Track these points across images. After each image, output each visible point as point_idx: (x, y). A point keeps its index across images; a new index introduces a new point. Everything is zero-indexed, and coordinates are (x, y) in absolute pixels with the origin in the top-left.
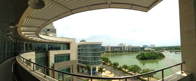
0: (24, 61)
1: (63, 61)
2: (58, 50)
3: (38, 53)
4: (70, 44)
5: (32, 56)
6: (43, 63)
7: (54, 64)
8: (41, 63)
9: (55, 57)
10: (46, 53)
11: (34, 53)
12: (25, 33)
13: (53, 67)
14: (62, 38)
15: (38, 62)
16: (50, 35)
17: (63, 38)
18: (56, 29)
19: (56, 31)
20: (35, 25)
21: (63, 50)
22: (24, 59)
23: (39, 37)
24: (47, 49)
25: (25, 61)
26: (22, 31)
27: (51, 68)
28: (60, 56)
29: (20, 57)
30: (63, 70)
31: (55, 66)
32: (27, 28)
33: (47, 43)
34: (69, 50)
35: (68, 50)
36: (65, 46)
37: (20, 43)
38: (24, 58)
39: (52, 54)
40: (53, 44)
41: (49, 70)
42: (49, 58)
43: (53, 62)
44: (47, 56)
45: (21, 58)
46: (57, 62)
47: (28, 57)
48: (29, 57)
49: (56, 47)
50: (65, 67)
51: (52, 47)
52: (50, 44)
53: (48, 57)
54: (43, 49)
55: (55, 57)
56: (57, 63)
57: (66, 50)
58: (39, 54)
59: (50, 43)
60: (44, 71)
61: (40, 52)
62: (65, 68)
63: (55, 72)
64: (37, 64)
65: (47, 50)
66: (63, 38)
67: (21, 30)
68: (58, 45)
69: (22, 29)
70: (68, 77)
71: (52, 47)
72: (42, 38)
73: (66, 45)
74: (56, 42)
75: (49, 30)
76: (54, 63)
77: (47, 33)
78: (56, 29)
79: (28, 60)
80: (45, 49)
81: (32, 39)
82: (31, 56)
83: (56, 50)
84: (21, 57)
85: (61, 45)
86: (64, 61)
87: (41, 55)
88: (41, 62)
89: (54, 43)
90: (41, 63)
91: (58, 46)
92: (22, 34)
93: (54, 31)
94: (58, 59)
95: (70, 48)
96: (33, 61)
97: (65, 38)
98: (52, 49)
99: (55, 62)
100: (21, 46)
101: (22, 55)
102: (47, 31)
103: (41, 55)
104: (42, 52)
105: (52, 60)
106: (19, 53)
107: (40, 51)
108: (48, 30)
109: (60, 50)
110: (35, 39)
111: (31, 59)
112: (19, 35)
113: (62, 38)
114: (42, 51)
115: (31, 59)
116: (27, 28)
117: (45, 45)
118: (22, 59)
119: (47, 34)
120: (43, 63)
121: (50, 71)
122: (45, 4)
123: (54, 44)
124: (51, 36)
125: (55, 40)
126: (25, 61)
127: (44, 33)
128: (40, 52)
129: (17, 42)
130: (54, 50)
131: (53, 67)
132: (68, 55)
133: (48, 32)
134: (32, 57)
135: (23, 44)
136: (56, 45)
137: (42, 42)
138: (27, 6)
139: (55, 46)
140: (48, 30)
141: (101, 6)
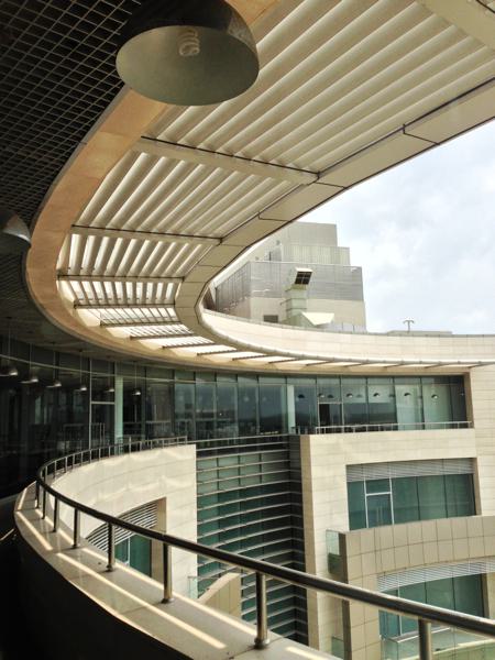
0: (84, 532)
1: (420, 519)
2: (372, 429)
3: (241, 450)
4: (469, 381)
5: (172, 477)
6: (263, 532)
7: (342, 537)
8: (243, 544)
9: (353, 488)
10: (287, 455)
11: (186, 454)
12: (96, 291)
13: (337, 564)
14: (400, 334)
15: (221, 537)
16: (315, 317)
17: (409, 333)
18: (359, 269)
19: (360, 286)
20: (172, 221)
21: (417, 428)
22: (83, 516)
23: (201, 329)
24: (292, 423)
25: (89, 525)
26: (63, 275)
27: (320, 571)
28: (391, 474)
29: (52, 499)
30: (426, 590)
31: (349, 553)
32: (91, 239)
33: (286, 376)
34: (465, 426)
35: (453, 426)
36: (427, 395)
37: (46, 380)
38: (79, 508)
39: (329, 462)
40: (336, 381)
41: (310, 590)
42: (305, 494)
43: (343, 524)
44: (289, 475)
45: (61, 504)
46: (374, 524)
47: (140, 489)
48: (151, 487)
49: (358, 405)
50: (440, 564)
51: (324, 409)
52: (312, 381)
53: (298, 487)
54: (257, 428)
55: (349, 484)
56: (367, 534)
57: (441, 427)
58: (228, 462)
59: (315, 377)
60: (254, 608)
61: (212, 444)
62: (445, 574)
63: (356, 607)
64: (214, 547)
65: (292, 432)
66: (409, 333)
67: (59, 266)
68: (379, 395)
69: (73, 250)
70: (462, 645)
71: (324, 409)
72: (218, 339)
73: (442, 389)
74: (354, 370)
75: (306, 282)
76: (344, 527)
77: (295, 303)
78: (359, 269)
79: (115, 514)
80: (277, 423)
81: (166, 354)
82: (164, 479)
83: (363, 430)
84: (58, 497)
85: (401, 389)
86: (427, 518)
87: (247, 469)
88: (243, 518)
89: (339, 377)
90: (243, 544)
91: (373, 400)
92: (56, 295)
93: (349, 286)
94: (377, 498)
95: (475, 417)
96: (182, 521)
97: (427, 335)
98: (329, 419)
99: (356, 520)
100: (85, 404)
101: (63, 483)
102: (139, 141)
103: (247, 469)
104: (254, 449)
105: (327, 513)
106: (41, 463)
107: (219, 443)
108: (303, 279)
109: (396, 429)
110: (189, 349)
111: (164, 500)
112: (38, 315)
113: (400, 334)
114: (254, 441)
115: (164, 500)
116: (91, 239)
117: (276, 396)
118: (66, 512)
119: (294, 312)
120: (263, 532)
121: (320, 602)
122: (258, 70)
123: (344, 381)
124: (320, 327)
125: (347, 357)
126: (89, 525)
127: (278, 301)
128: (212, 444)
129: (28, 377)
130: (350, 430)
131: (337, 564)
132: (462, 469)
133: (296, 294)
134: (173, 483)
135: (103, 391)
136: (363, 394)
137: (255, 375)
138: (114, 86)
139: (342, 403)
140: (298, 281)
141: (407, 380)
